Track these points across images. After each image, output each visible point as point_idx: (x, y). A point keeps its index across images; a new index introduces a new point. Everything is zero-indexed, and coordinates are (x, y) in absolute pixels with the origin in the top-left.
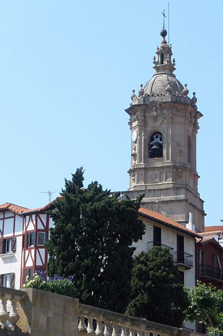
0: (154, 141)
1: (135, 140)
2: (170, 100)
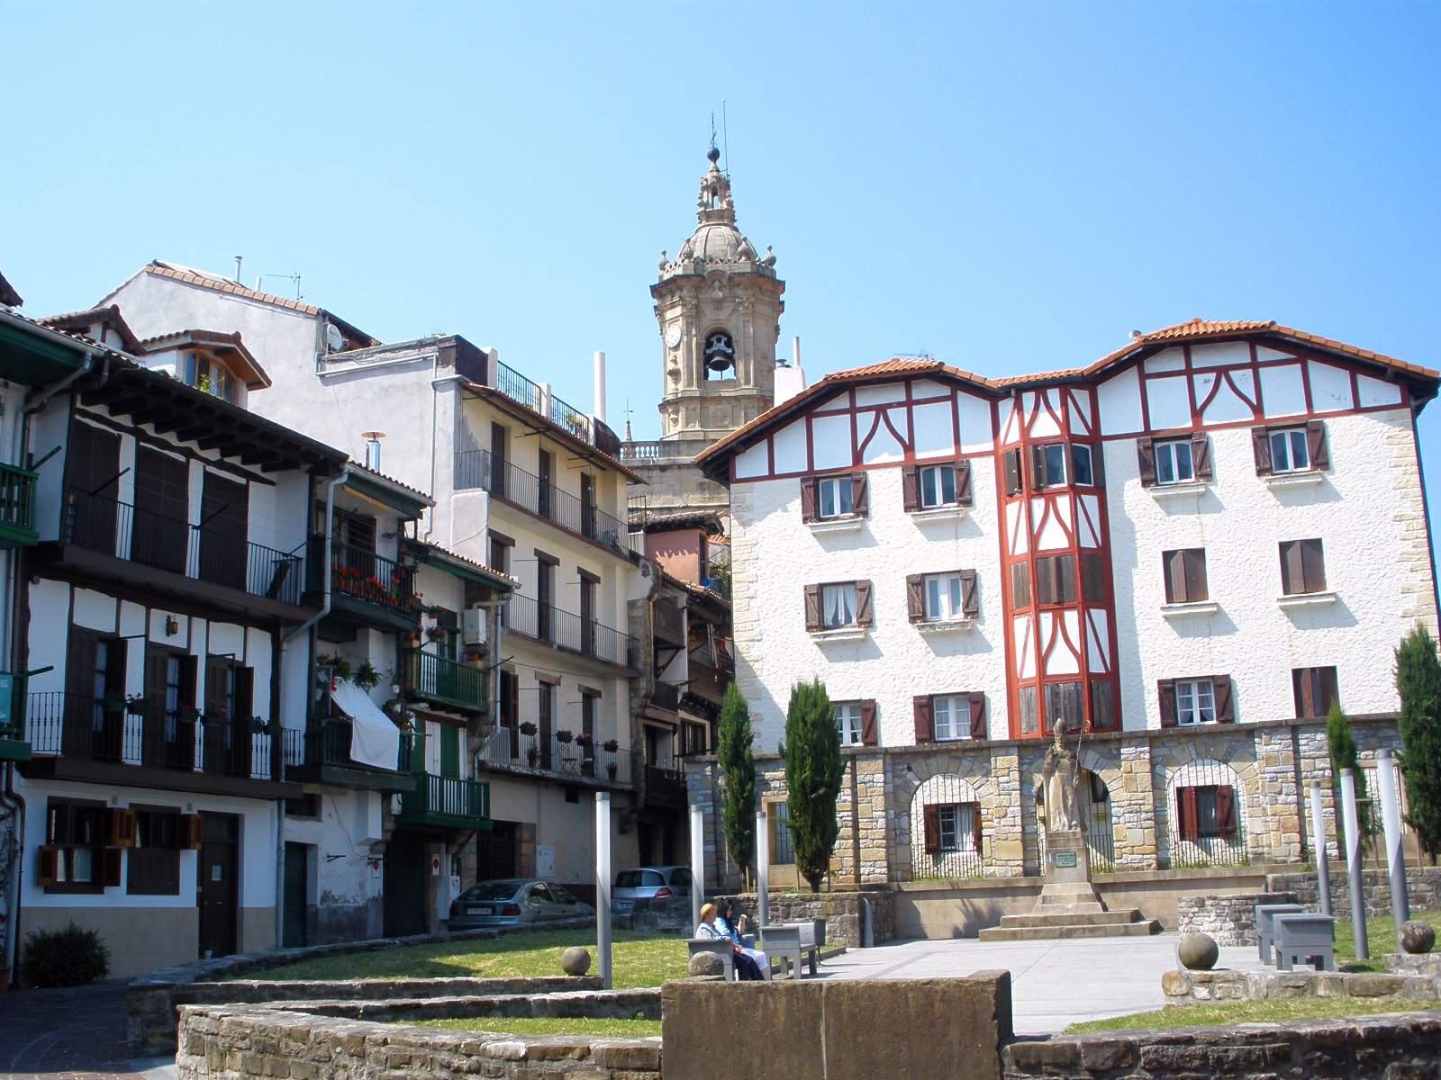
0: (715, 348)
1: (675, 344)
2: (749, 270)
